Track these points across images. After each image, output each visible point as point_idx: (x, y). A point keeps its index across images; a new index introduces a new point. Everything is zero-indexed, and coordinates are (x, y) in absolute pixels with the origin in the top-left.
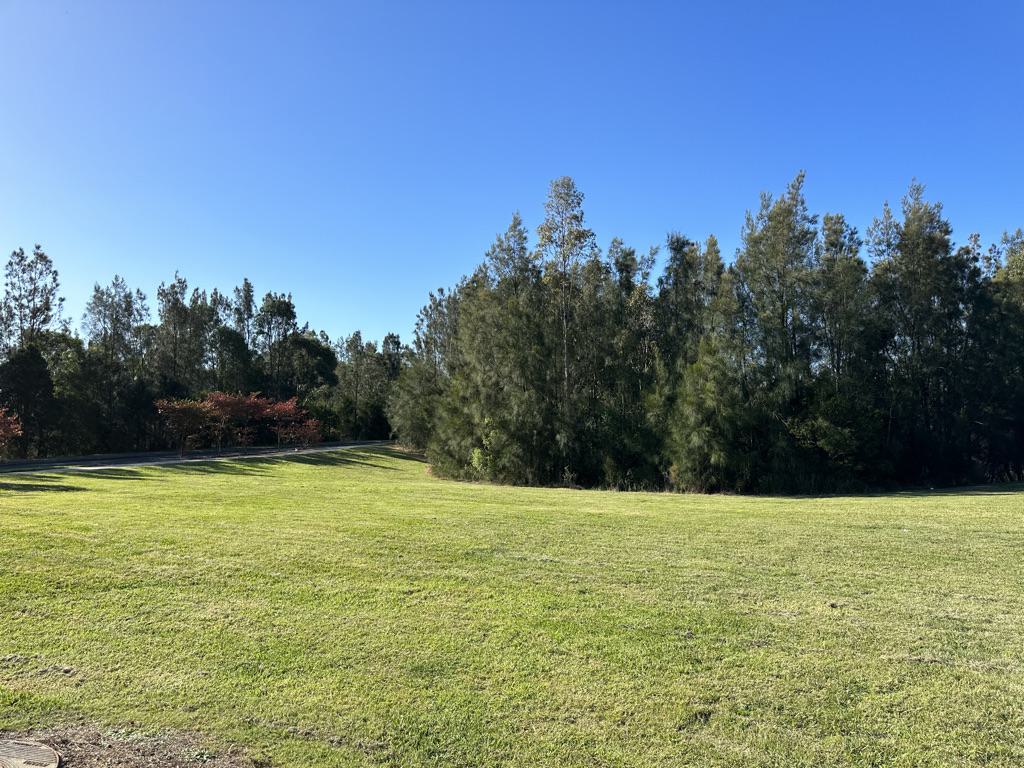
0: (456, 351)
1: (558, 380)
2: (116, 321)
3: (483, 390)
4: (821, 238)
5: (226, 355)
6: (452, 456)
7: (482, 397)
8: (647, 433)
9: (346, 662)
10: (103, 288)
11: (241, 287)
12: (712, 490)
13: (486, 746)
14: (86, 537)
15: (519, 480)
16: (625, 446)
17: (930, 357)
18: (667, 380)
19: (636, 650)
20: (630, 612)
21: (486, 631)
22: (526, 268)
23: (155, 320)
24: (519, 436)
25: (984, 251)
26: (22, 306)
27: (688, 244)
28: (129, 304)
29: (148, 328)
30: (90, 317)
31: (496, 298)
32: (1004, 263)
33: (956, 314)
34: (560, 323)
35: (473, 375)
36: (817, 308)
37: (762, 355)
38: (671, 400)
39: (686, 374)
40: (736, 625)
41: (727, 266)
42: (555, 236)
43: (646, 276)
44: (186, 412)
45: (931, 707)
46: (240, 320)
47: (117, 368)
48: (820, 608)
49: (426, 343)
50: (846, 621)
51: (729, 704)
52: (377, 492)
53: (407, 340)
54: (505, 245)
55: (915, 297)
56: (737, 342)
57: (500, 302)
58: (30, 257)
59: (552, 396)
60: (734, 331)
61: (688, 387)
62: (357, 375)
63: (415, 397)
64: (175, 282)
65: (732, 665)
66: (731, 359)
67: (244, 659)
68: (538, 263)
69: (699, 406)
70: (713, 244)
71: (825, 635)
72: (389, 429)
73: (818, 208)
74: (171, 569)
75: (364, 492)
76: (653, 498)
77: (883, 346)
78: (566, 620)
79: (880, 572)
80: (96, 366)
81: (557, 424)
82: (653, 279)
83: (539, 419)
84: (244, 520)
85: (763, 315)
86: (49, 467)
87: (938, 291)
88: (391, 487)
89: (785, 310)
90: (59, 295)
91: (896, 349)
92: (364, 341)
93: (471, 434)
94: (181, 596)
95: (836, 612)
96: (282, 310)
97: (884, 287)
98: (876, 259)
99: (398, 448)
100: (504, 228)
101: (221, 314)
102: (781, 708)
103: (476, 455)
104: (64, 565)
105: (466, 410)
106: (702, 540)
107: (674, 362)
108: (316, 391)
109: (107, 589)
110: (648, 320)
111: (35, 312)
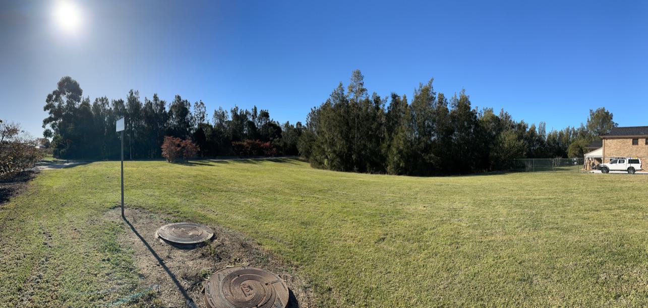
0: (320, 127)
1: (353, 138)
2: (220, 120)
3: (328, 140)
4: (437, 100)
5: (250, 129)
6: (317, 161)
7: (328, 142)
8: (381, 156)
9: (283, 219)
10: (217, 110)
11: (253, 108)
12: (400, 174)
13: (320, 246)
14: (216, 178)
15: (339, 169)
16: (373, 160)
17: (463, 138)
18: (389, 140)
19: (367, 220)
20: (367, 209)
21: (323, 213)
22: (344, 101)
23: (230, 119)
24: (340, 155)
25: (479, 112)
26: (198, 117)
27: (397, 96)
28: (224, 115)
29: (228, 121)
30: (214, 119)
31: (332, 110)
32: (483, 116)
33: (470, 128)
34: (355, 119)
35: (325, 135)
36: (434, 121)
37: (417, 134)
38: (389, 146)
39: (394, 138)
40: (397, 212)
41: (409, 105)
42: (354, 90)
43: (384, 105)
44: (240, 145)
45: (442, 233)
46: (253, 119)
47: (221, 133)
48: (421, 208)
49: (310, 125)
50: (427, 211)
51: (390, 235)
52: (293, 171)
53: (304, 124)
54: (337, 92)
55: (461, 121)
56: (410, 129)
57: (335, 111)
58: (199, 104)
59: (351, 142)
60: (409, 126)
61: (395, 142)
62: (288, 135)
63: (306, 142)
64: (235, 107)
65: (394, 224)
66: (409, 134)
67: (255, 215)
68: (347, 98)
69: (398, 148)
70: (405, 97)
71: (419, 215)
72: (298, 152)
73: (437, 90)
74: (236, 188)
75: (289, 171)
76: (282, 168)
77: (452, 135)
78: (347, 211)
79: (439, 197)
80: (216, 132)
81: (352, 152)
82: (386, 106)
83: (346, 150)
84: (255, 176)
85: (418, 121)
86: (206, 159)
87: (466, 120)
88: (298, 170)
89: (425, 120)
90: (206, 113)
91: (455, 136)
92: (290, 124)
93: (324, 154)
94: (239, 196)
95: (425, 209)
96: (265, 115)
97: (453, 117)
98: (451, 109)
99: (301, 158)
100: (336, 86)
101: (248, 117)
102: (404, 236)
103: (326, 161)
104: (211, 184)
105: (322, 146)
106: (393, 189)
107: (391, 134)
108: (275, 140)
109: (222, 192)
110: (383, 120)
111: (201, 118)
